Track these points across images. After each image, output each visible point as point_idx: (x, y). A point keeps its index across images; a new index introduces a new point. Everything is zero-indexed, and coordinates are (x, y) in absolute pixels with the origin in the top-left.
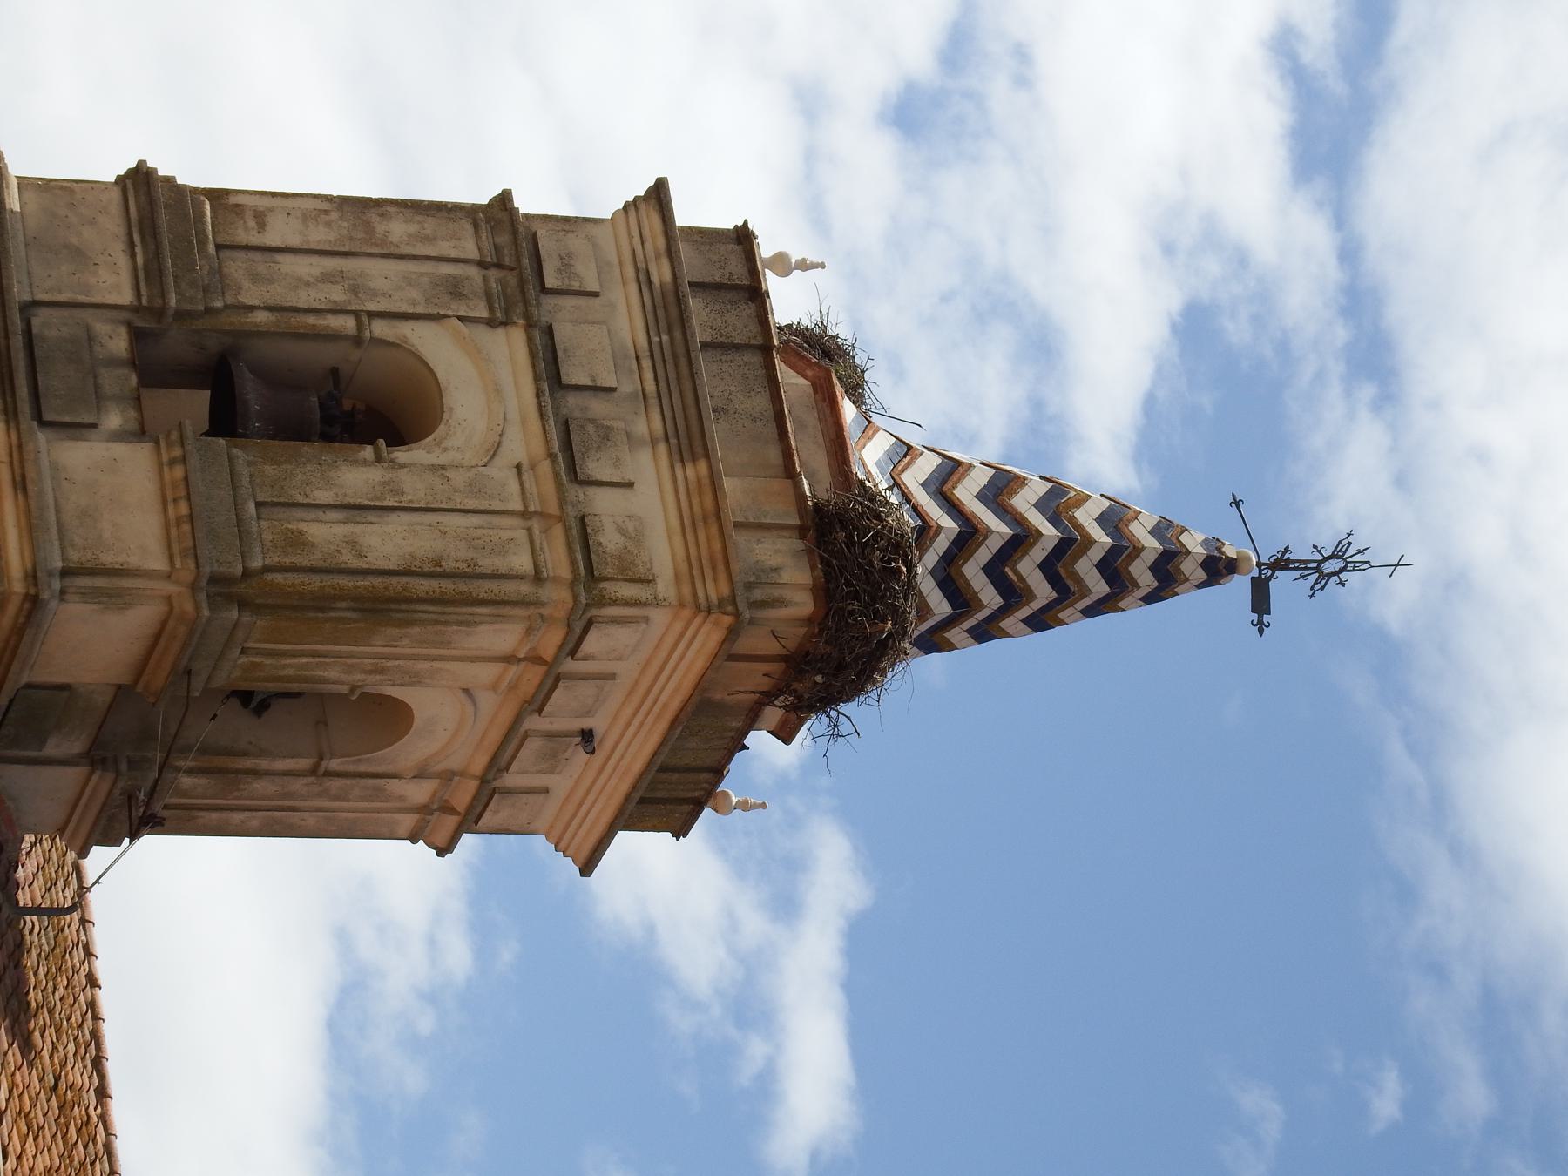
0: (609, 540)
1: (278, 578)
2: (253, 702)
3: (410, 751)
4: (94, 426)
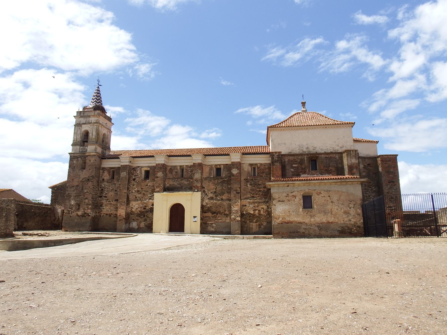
2: (103, 141)
3: (106, 134)
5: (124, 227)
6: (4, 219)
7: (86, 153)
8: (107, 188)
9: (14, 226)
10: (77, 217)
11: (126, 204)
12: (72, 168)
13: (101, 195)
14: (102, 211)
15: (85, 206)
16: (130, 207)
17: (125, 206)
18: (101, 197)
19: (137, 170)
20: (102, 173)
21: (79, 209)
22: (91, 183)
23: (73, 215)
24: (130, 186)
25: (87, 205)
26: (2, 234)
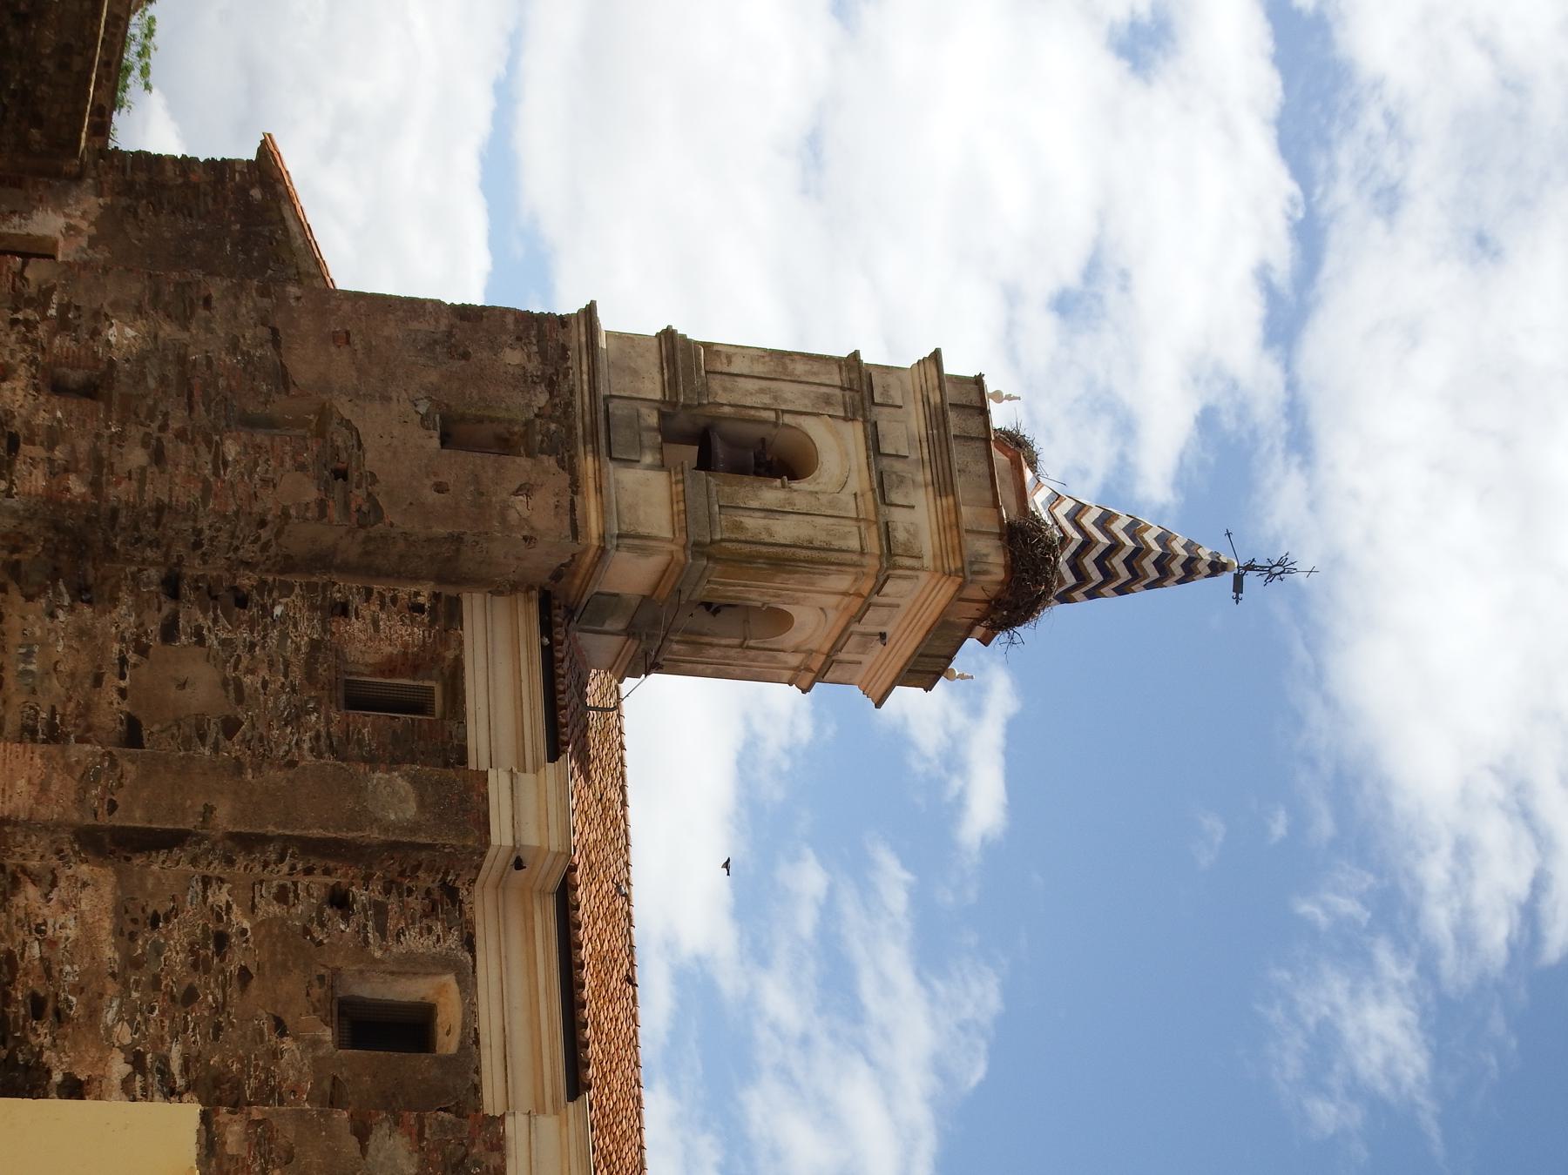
0: (900, 535)
1: (729, 545)
2: (712, 608)
3: (791, 638)
4: (638, 461)
7: (596, 453)
8: (252, 646)
11: (90, 821)
12: (450, 334)
13: (185, 589)
15: (83, 446)
16: (54, 861)
17: (76, 816)
18: (172, 586)
19: (438, 928)
21: (58, 388)
22: (312, 494)
24: (273, 857)
25: (98, 462)
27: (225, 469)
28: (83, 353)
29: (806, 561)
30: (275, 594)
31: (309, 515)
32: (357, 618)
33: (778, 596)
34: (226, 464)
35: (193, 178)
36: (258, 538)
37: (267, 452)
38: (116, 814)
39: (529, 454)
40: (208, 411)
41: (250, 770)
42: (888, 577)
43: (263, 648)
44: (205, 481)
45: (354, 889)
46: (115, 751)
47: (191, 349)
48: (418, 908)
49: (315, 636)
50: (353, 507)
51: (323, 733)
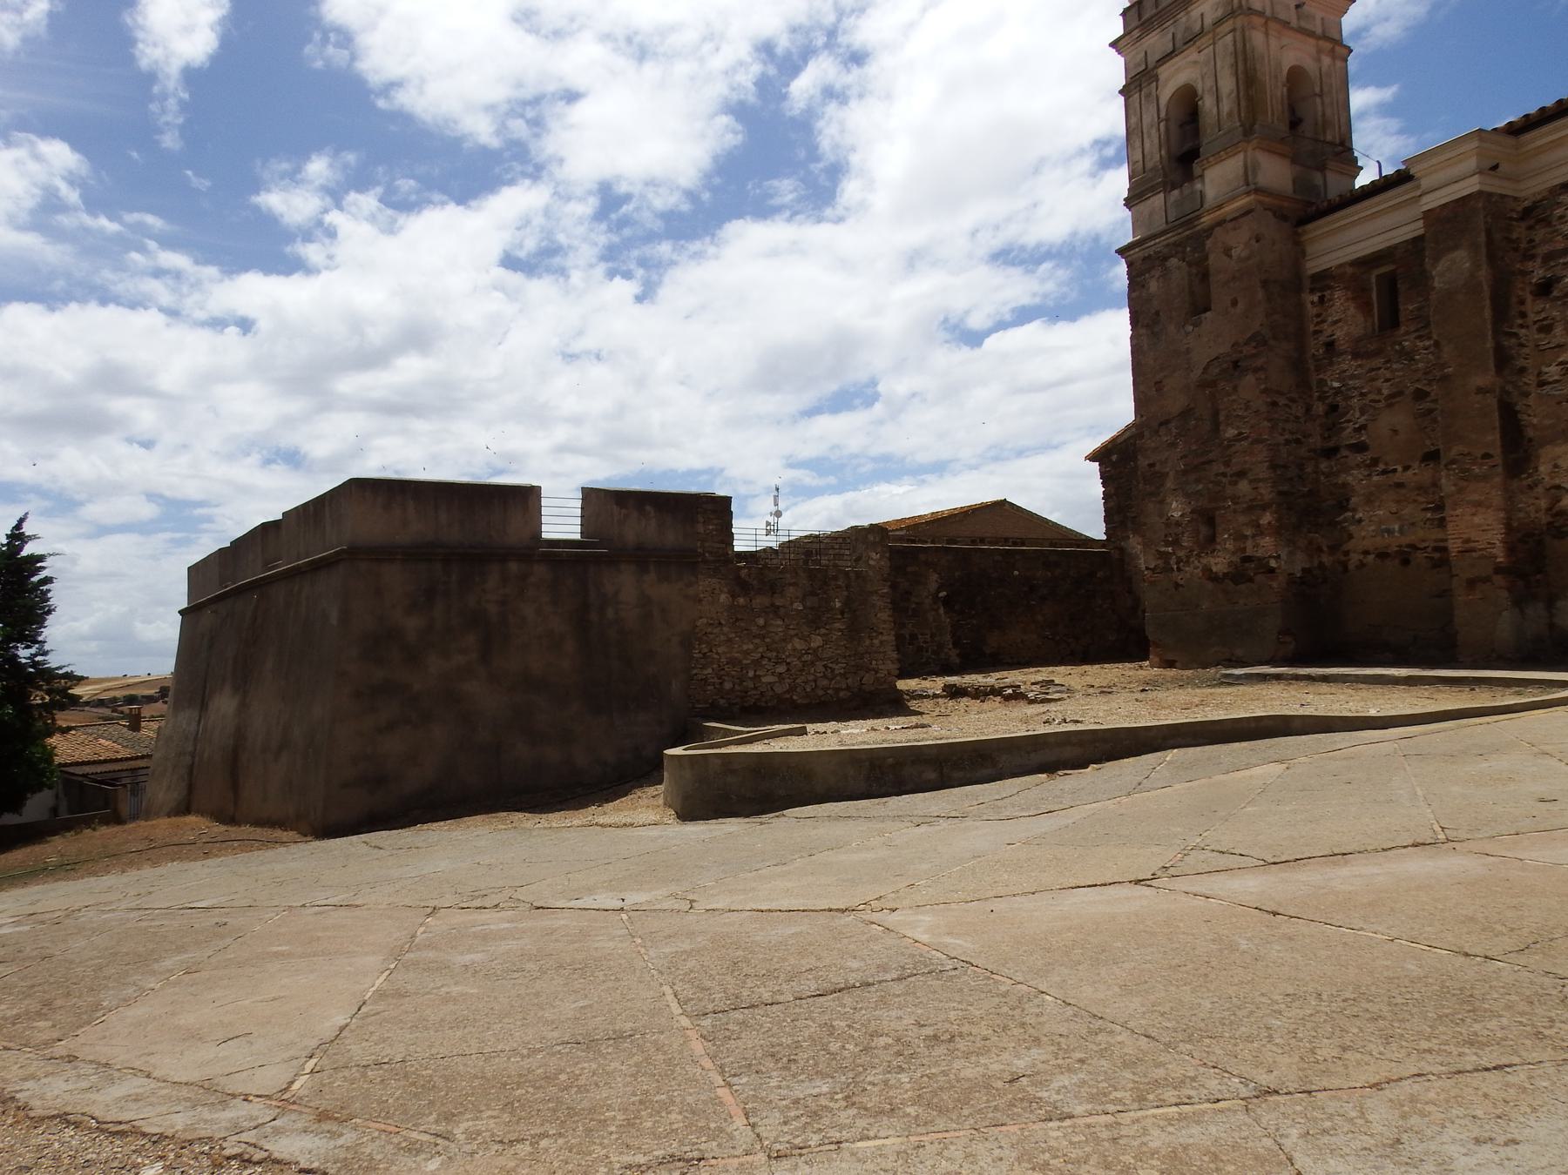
0: (1220, 13)
1: (1243, 115)
2: (1295, 124)
3: (1309, 65)
4: (1201, 192)
5: (1505, 626)
6: (837, 625)
7: (1199, 217)
8: (1362, 395)
9: (895, 655)
10: (1210, 585)
11: (1500, 469)
12: (1147, 326)
13: (1331, 444)
14: (1351, 537)
15: (1242, 519)
16: (1540, 490)
17: (1497, 480)
18: (1330, 453)
19: (1558, 212)
20: (1315, 311)
21: (1212, 539)
22: (1250, 379)
23: (1188, 575)
24: (1513, 341)
25: (1250, 509)
26: (842, 694)
27: (1243, 434)
28: (1190, 529)
29: (1246, 64)
30: (1326, 389)
31: (1263, 377)
32: (1333, 335)
33: (1276, 77)
34: (1240, 434)
35: (1113, 491)
36: (1286, 405)
37: (1229, 411)
38: (1491, 452)
39: (1206, 258)
40: (1211, 451)
41: (1446, 371)
42: (1250, 9)
43: (1362, 388)
44: (1252, 443)
45: (1534, 280)
46: (1443, 462)
47: (1178, 469)
48: (1543, 231)
49: (1350, 357)
50: (1254, 351)
51: (1417, 334)
